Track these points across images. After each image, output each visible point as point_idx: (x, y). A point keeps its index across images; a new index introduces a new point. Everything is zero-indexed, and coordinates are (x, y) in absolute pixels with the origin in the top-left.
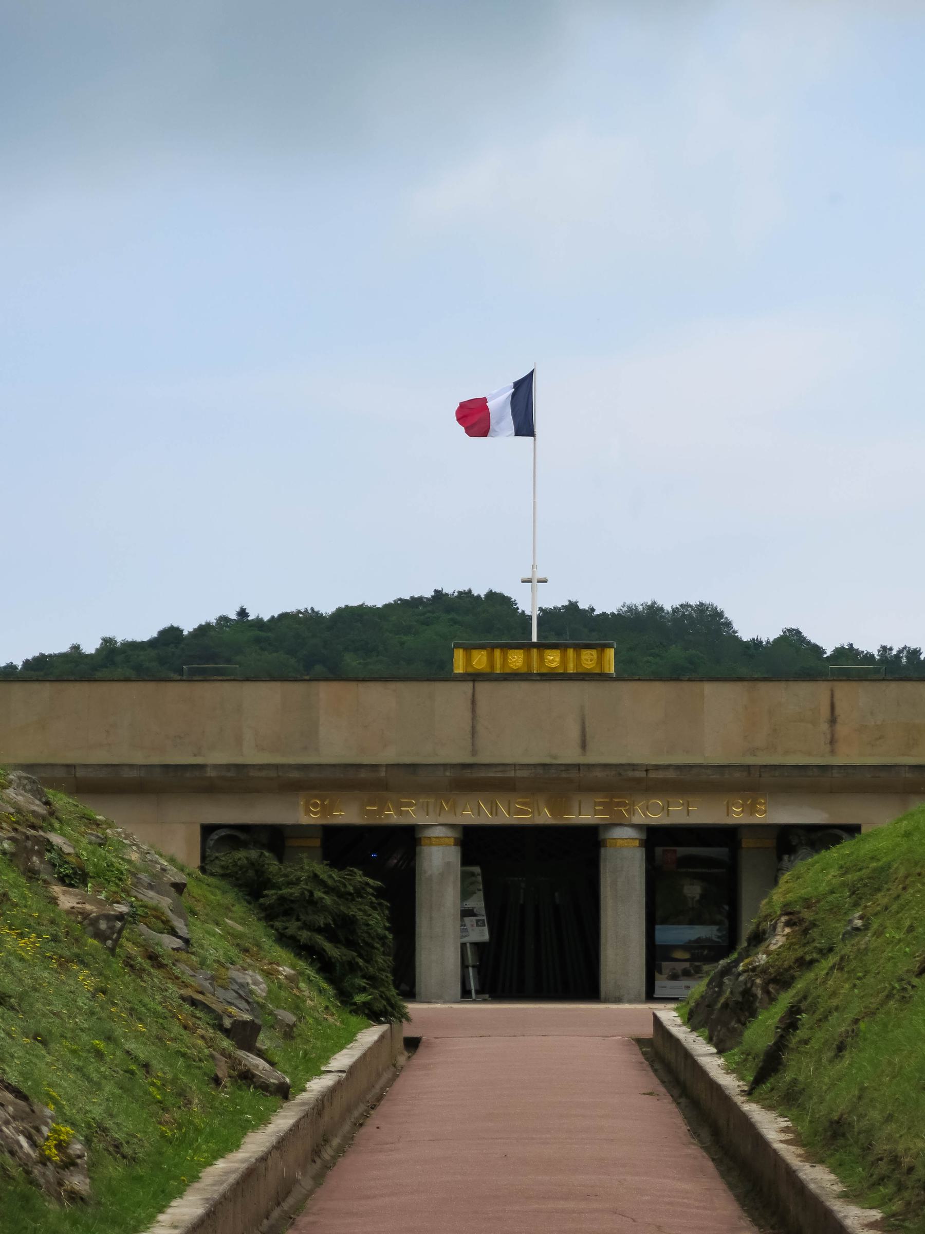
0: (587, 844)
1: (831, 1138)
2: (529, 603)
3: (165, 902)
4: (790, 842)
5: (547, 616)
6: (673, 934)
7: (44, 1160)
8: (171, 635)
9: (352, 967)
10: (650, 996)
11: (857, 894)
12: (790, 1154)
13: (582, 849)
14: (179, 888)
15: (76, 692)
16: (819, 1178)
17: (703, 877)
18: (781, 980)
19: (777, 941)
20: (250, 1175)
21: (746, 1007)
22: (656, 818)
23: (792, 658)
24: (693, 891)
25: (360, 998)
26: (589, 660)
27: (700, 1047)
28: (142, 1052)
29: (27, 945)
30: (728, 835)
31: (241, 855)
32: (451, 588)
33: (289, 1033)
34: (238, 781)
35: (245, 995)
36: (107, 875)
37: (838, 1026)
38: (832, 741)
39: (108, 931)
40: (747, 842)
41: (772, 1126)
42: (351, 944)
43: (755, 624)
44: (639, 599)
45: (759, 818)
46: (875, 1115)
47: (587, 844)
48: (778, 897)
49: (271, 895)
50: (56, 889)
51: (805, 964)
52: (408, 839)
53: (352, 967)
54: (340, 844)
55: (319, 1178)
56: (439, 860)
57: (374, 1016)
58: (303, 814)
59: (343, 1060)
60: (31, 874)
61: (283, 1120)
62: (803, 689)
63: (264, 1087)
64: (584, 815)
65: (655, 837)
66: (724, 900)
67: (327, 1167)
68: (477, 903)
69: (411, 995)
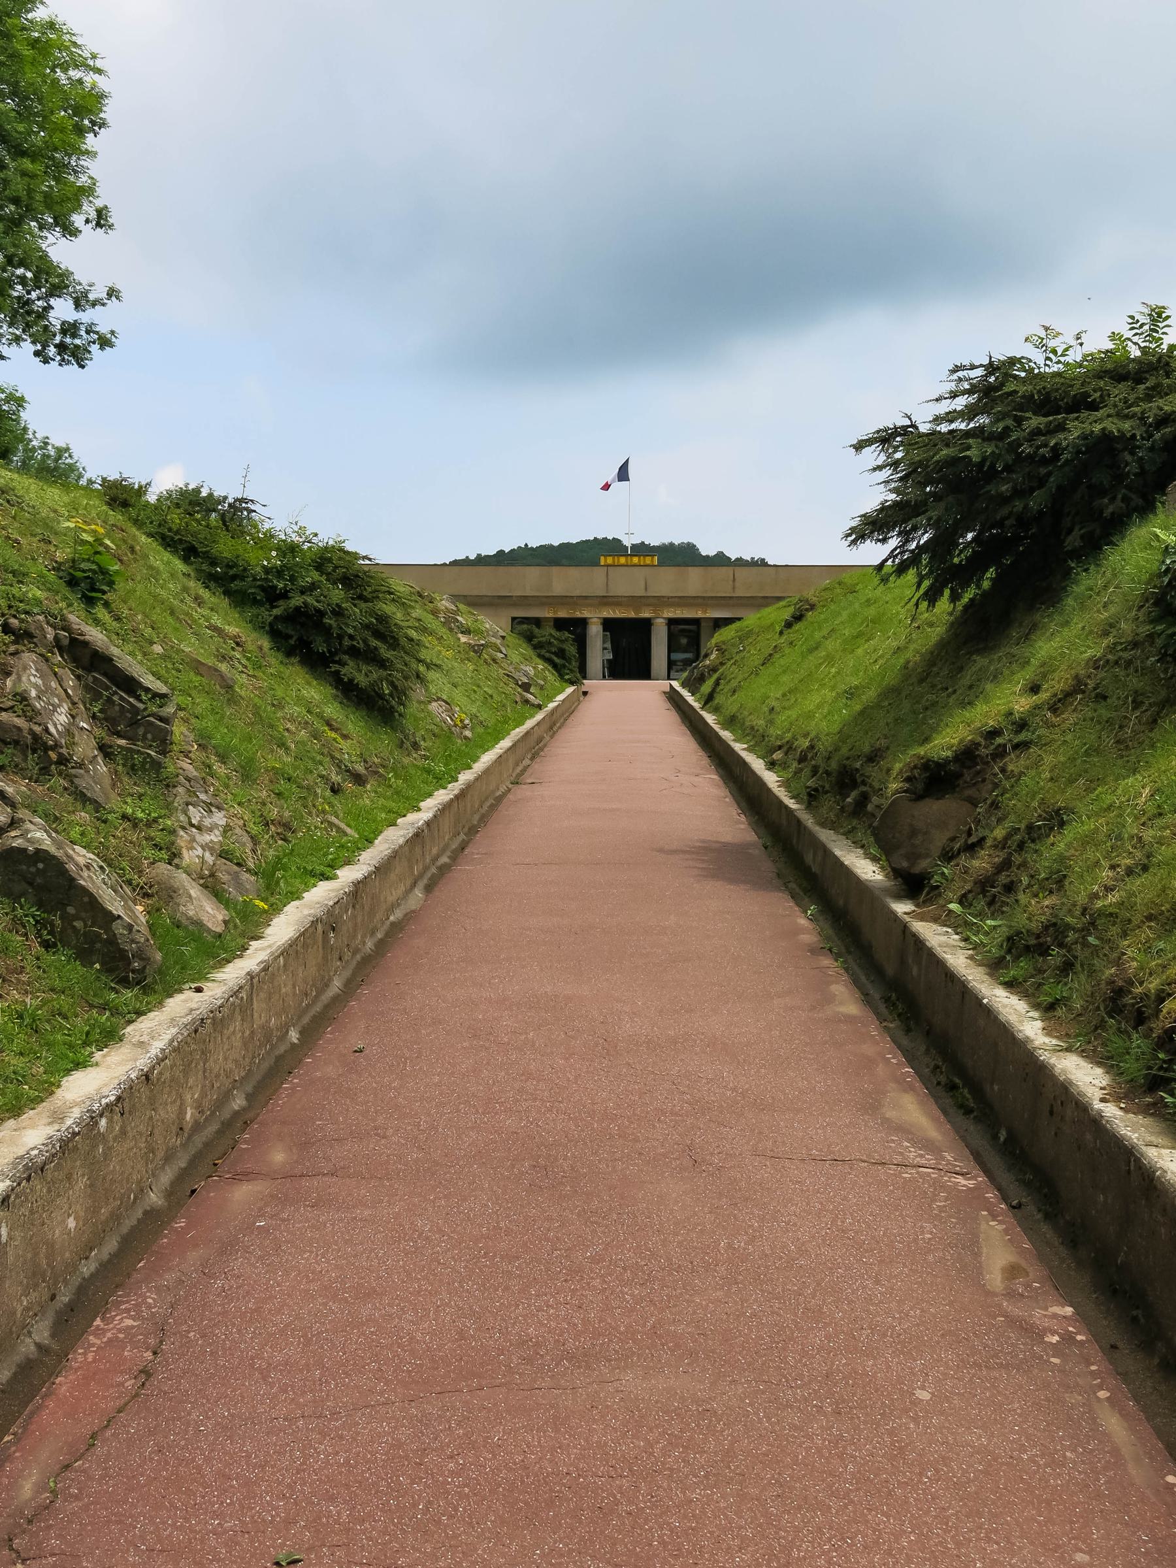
0: (647, 624)
1: (730, 722)
2: (628, 542)
3: (498, 642)
4: (718, 623)
5: (633, 546)
6: (677, 656)
7: (456, 725)
8: (501, 552)
9: (564, 666)
10: (669, 678)
11: (741, 639)
12: (716, 727)
13: (645, 626)
14: (503, 637)
15: (467, 569)
16: (726, 735)
17: (688, 637)
18: (714, 670)
19: (713, 657)
20: (527, 733)
21: (702, 679)
22: (671, 615)
23: (720, 560)
24: (684, 641)
25: (567, 677)
26: (648, 560)
27: (685, 693)
28: (490, 692)
29: (450, 653)
30: (696, 622)
31: (525, 626)
32: (600, 537)
33: (542, 688)
34: (524, 601)
35: (526, 675)
36: (479, 632)
37: (734, 684)
38: (734, 588)
39: (478, 650)
40: (703, 624)
41: (710, 718)
42: (564, 658)
43: (707, 549)
44: (667, 541)
45: (708, 615)
46: (746, 713)
47: (647, 624)
48: (713, 641)
49: (535, 641)
50: (460, 635)
51: (722, 664)
52: (583, 623)
53: (564, 666)
54: (560, 624)
55: (552, 737)
56: (595, 630)
57: (572, 683)
58: (547, 613)
59: (560, 697)
60: (451, 630)
61: (539, 716)
62: (724, 569)
63: (533, 705)
64: (646, 614)
65: (671, 622)
66: (695, 644)
67: (554, 733)
68: (608, 645)
69: (585, 678)
